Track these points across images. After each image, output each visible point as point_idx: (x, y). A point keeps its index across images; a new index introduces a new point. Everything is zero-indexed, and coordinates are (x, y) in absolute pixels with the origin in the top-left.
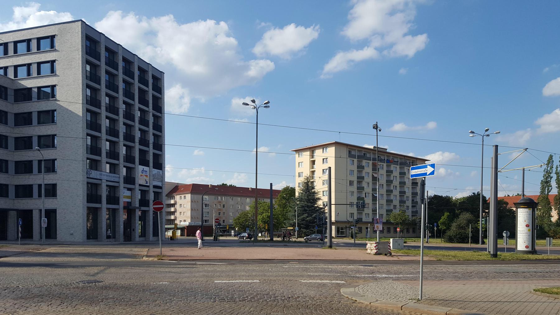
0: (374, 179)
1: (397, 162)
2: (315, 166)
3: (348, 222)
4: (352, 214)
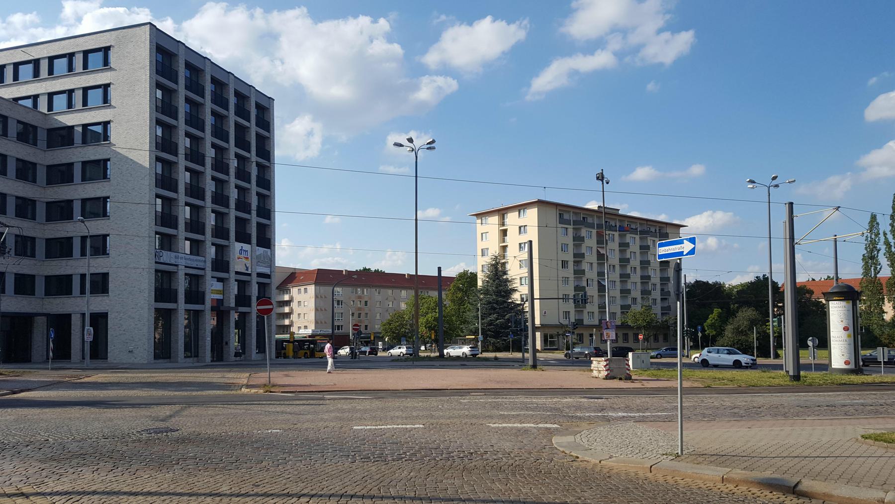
0: (601, 257)
1: (636, 229)
2: (507, 238)
3: (561, 326)
4: (567, 314)
